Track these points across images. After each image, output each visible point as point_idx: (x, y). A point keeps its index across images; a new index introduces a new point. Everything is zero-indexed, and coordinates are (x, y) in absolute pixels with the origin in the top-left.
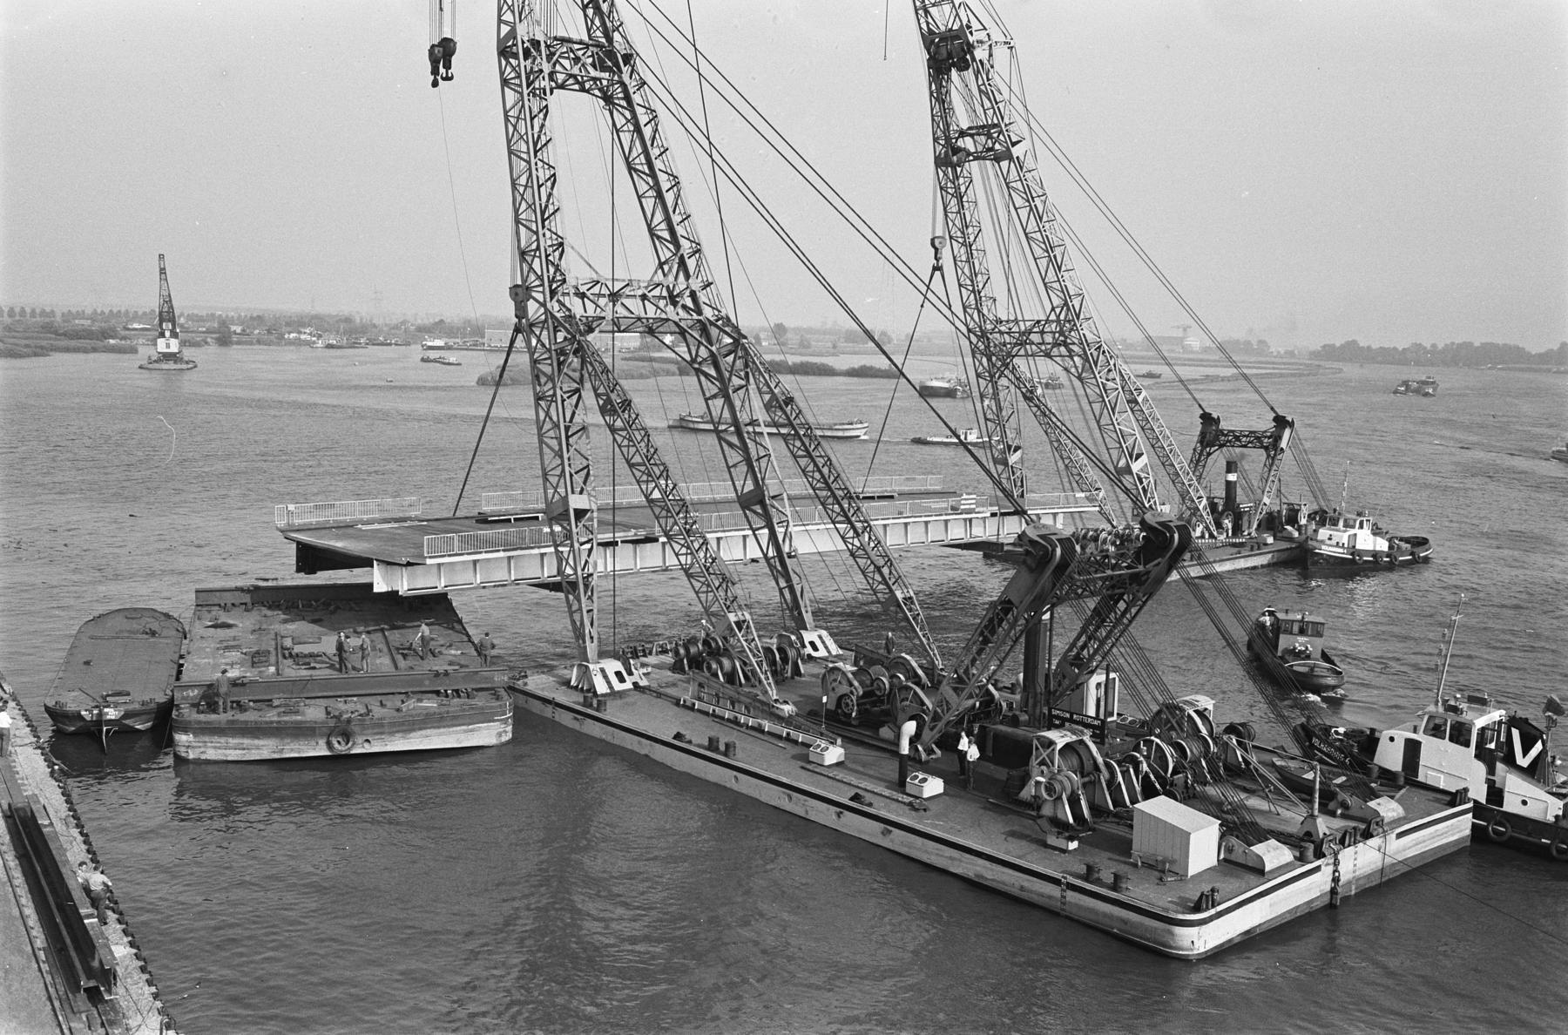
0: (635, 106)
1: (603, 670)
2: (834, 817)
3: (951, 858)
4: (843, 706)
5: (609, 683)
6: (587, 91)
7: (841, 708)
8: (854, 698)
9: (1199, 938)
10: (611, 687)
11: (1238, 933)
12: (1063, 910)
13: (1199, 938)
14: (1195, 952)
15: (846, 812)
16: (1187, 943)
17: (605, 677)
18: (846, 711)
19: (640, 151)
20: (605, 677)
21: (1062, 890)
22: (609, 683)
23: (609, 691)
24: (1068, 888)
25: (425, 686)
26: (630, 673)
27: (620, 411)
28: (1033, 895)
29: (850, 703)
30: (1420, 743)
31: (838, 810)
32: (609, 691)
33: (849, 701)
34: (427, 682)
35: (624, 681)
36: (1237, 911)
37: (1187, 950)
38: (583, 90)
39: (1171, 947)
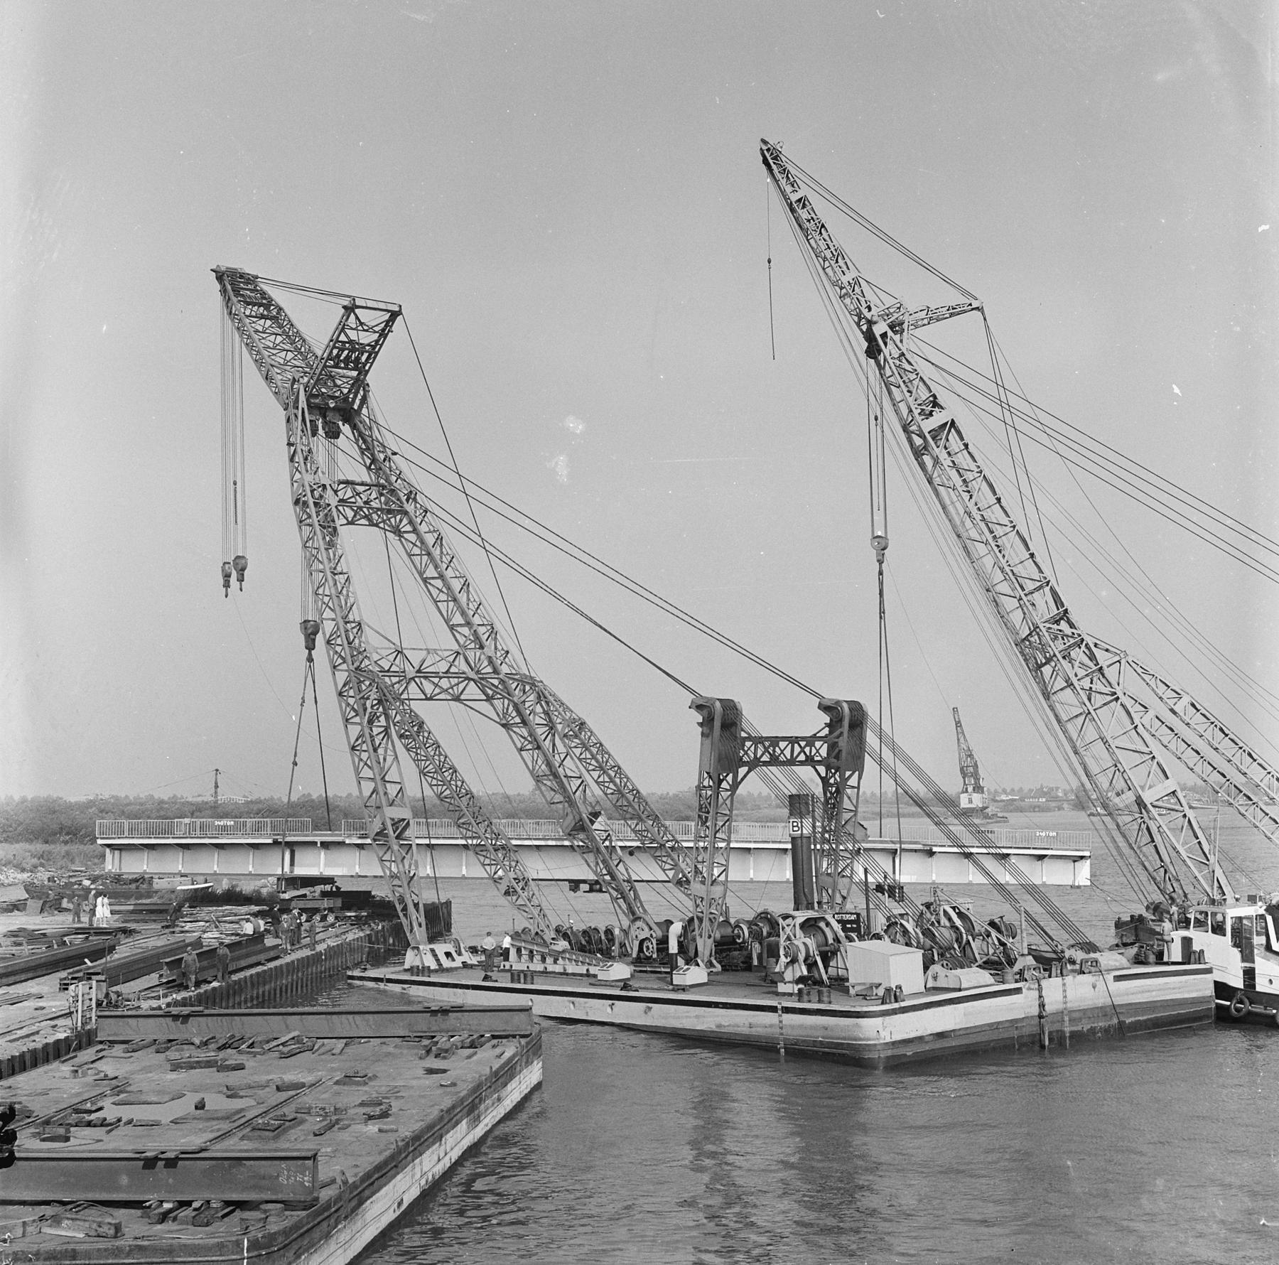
0: (449, 580)
1: (433, 951)
2: (609, 1009)
3: (697, 1017)
4: (645, 950)
5: (438, 960)
6: (376, 525)
7: (643, 952)
8: (654, 942)
9: (884, 1028)
10: (440, 965)
11: (929, 1032)
12: (782, 1034)
13: (884, 1028)
14: (882, 1042)
15: (616, 1002)
16: (873, 1034)
17: (435, 956)
18: (647, 954)
19: (749, 752)
20: (435, 956)
21: (780, 1016)
22: (438, 960)
23: (437, 967)
24: (783, 1012)
25: (118, 1189)
26: (460, 954)
27: (519, 889)
28: (758, 1029)
29: (651, 946)
30: (1192, 939)
31: (610, 1002)
32: (437, 967)
33: (649, 944)
34: (124, 1180)
35: (453, 960)
36: (925, 1011)
37: (873, 1040)
38: (372, 524)
39: (861, 1039)
